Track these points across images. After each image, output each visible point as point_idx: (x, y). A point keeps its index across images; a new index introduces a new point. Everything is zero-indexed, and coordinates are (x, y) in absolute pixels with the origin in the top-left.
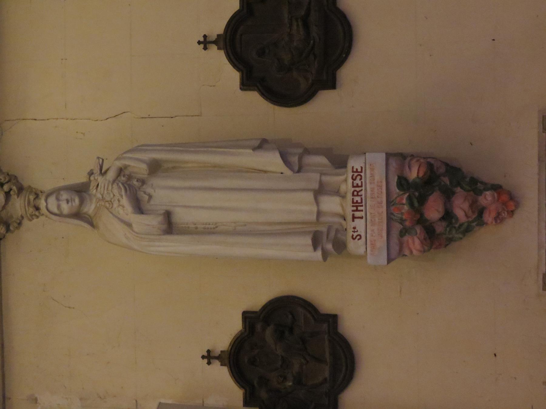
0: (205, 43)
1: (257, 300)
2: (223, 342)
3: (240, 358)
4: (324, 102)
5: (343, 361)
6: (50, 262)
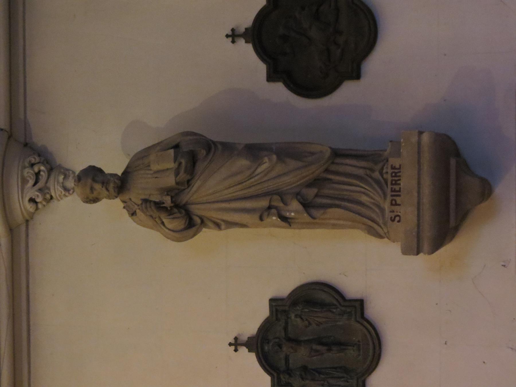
0: (233, 36)
1: (284, 288)
2: (251, 328)
3: (266, 345)
4: (348, 92)
5: (371, 347)
6: (88, 247)
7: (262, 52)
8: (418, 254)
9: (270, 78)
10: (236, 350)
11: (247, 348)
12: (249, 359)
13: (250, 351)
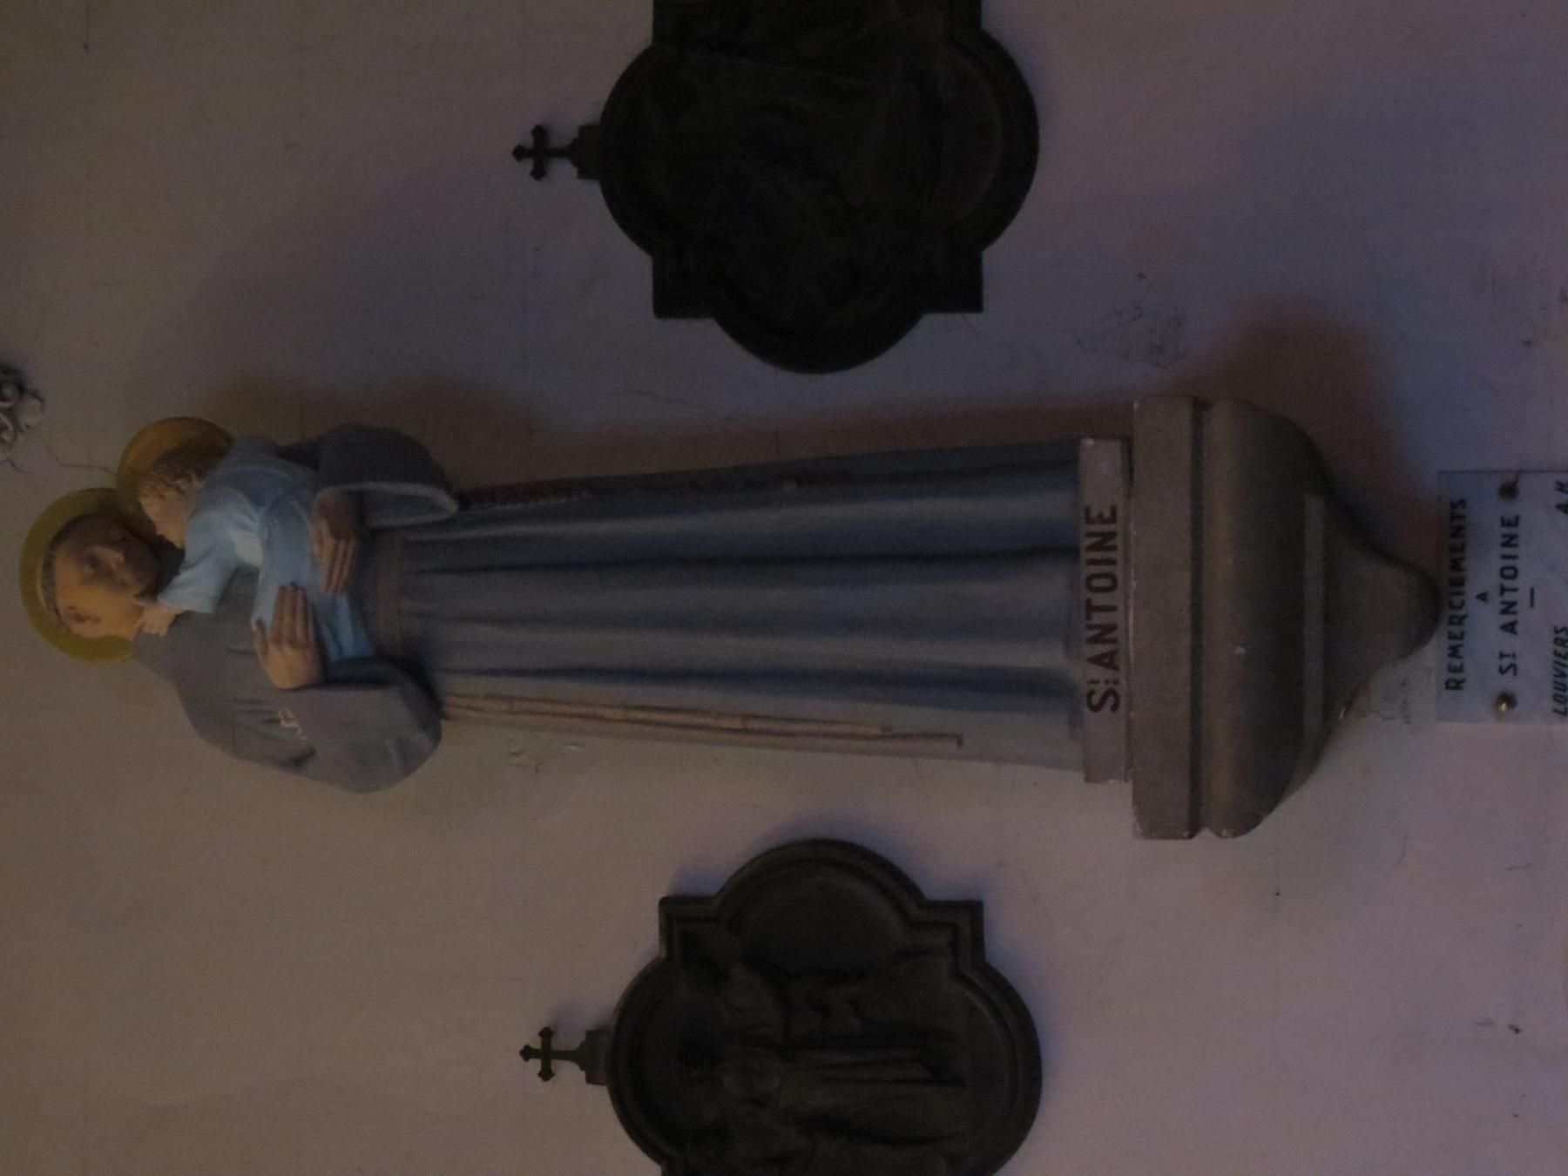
3: (646, 1056)
7: (636, 212)
8: (1193, 831)
9: (671, 299)
10: (546, 1074)
11: (575, 164)
12: (586, 1104)
13: (584, 173)
